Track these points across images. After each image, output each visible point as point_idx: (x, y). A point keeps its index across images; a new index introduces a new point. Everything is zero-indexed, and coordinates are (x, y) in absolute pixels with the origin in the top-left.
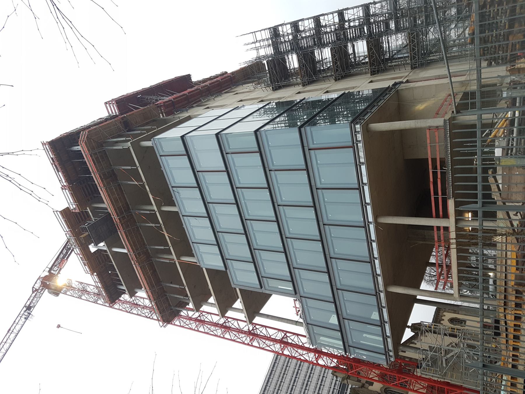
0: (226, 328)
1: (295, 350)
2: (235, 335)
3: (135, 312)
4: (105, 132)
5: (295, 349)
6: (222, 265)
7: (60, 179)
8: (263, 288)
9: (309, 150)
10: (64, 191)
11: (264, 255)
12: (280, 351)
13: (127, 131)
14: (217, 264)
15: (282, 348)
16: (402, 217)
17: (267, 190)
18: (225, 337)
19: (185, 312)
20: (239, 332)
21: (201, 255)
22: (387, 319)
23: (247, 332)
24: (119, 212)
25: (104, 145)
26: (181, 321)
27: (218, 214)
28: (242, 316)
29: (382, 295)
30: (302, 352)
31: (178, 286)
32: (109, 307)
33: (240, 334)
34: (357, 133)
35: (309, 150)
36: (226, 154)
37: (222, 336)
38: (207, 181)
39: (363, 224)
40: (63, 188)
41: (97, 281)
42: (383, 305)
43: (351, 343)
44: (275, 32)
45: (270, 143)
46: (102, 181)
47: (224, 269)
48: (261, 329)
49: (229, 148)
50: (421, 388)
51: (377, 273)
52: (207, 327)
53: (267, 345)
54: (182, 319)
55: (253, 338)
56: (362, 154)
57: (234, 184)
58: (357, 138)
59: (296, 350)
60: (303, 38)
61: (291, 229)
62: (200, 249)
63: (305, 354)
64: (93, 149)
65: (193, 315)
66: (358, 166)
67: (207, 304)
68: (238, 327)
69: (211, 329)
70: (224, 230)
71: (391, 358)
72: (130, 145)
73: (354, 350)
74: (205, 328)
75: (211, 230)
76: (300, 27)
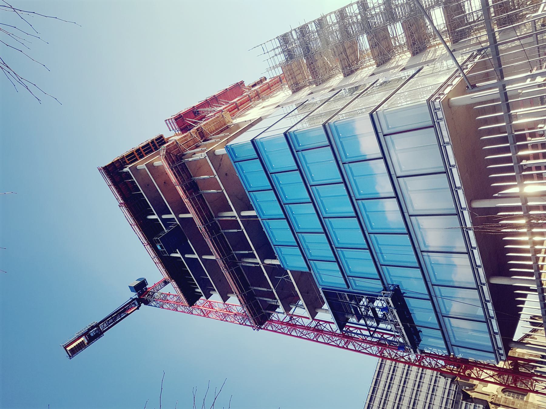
0: (318, 331)
1: (395, 352)
2: (328, 338)
3: (270, 328)
4: (183, 145)
5: (394, 351)
6: (306, 266)
7: (117, 198)
8: (351, 288)
9: (384, 135)
10: (121, 207)
11: (347, 253)
12: (378, 353)
13: (203, 141)
14: (300, 264)
15: (380, 350)
16: (483, 200)
17: (343, 184)
18: (319, 340)
19: (276, 315)
20: (332, 335)
21: (284, 257)
22: (493, 314)
23: (340, 334)
24: (204, 221)
25: (183, 157)
26: (273, 326)
27: (296, 214)
28: (305, 312)
29: (485, 288)
30: (402, 353)
31: (265, 289)
32: (203, 316)
33: (333, 337)
34: (437, 110)
35: (384, 135)
36: (296, 152)
37: (316, 340)
38: (281, 182)
39: (455, 212)
40: (120, 205)
41: (176, 287)
42: (487, 299)
43: (454, 342)
44: (285, 39)
45: (341, 135)
46: (185, 192)
47: (307, 270)
48: (324, 325)
49: (299, 146)
50: (488, 377)
51: (477, 264)
52: (299, 331)
53: (363, 347)
54: (274, 324)
55: (347, 341)
56: (445, 133)
57: (307, 182)
58: (438, 116)
59: (396, 352)
60: (397, 6)
61: (373, 224)
62: (283, 251)
63: (406, 356)
64: (173, 162)
65: (284, 319)
66: (442, 147)
67: (322, 311)
68: (331, 330)
69: (303, 333)
70: (313, 230)
71: (501, 357)
72: (206, 155)
73: (458, 350)
74: (298, 332)
75: (290, 231)
76: (369, 4)
